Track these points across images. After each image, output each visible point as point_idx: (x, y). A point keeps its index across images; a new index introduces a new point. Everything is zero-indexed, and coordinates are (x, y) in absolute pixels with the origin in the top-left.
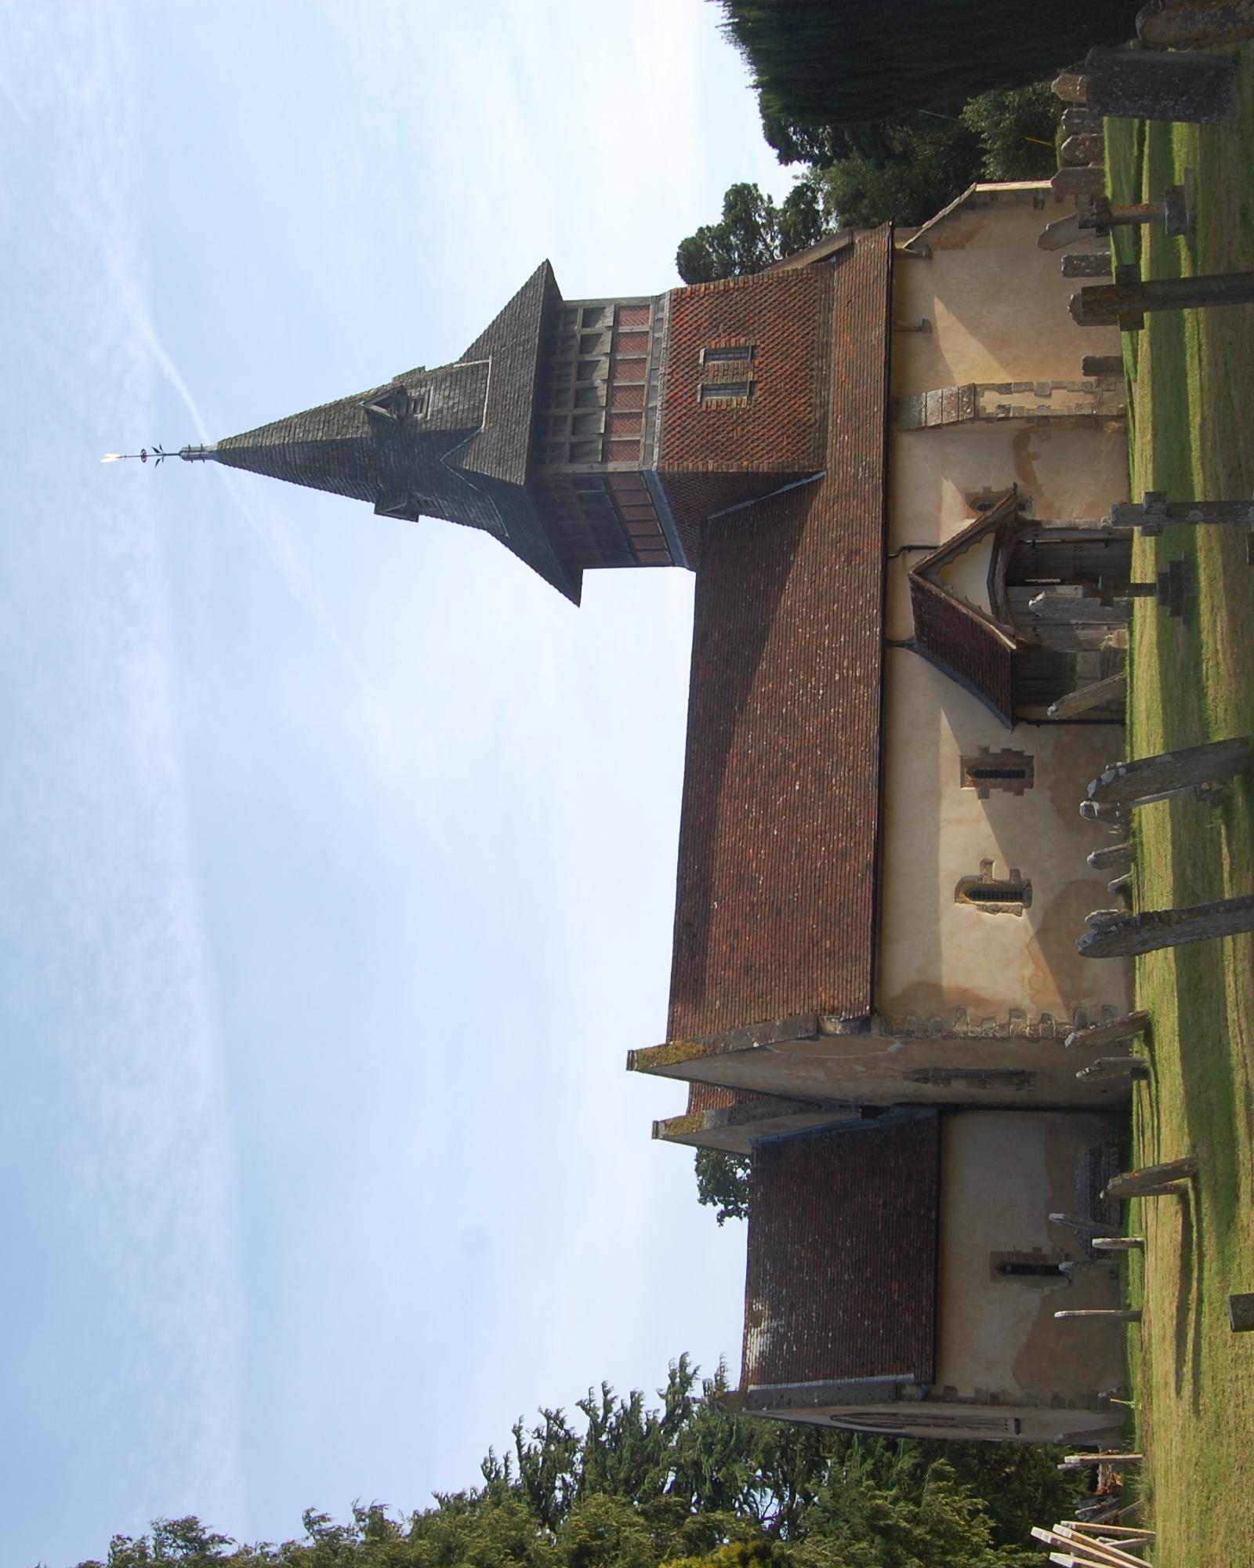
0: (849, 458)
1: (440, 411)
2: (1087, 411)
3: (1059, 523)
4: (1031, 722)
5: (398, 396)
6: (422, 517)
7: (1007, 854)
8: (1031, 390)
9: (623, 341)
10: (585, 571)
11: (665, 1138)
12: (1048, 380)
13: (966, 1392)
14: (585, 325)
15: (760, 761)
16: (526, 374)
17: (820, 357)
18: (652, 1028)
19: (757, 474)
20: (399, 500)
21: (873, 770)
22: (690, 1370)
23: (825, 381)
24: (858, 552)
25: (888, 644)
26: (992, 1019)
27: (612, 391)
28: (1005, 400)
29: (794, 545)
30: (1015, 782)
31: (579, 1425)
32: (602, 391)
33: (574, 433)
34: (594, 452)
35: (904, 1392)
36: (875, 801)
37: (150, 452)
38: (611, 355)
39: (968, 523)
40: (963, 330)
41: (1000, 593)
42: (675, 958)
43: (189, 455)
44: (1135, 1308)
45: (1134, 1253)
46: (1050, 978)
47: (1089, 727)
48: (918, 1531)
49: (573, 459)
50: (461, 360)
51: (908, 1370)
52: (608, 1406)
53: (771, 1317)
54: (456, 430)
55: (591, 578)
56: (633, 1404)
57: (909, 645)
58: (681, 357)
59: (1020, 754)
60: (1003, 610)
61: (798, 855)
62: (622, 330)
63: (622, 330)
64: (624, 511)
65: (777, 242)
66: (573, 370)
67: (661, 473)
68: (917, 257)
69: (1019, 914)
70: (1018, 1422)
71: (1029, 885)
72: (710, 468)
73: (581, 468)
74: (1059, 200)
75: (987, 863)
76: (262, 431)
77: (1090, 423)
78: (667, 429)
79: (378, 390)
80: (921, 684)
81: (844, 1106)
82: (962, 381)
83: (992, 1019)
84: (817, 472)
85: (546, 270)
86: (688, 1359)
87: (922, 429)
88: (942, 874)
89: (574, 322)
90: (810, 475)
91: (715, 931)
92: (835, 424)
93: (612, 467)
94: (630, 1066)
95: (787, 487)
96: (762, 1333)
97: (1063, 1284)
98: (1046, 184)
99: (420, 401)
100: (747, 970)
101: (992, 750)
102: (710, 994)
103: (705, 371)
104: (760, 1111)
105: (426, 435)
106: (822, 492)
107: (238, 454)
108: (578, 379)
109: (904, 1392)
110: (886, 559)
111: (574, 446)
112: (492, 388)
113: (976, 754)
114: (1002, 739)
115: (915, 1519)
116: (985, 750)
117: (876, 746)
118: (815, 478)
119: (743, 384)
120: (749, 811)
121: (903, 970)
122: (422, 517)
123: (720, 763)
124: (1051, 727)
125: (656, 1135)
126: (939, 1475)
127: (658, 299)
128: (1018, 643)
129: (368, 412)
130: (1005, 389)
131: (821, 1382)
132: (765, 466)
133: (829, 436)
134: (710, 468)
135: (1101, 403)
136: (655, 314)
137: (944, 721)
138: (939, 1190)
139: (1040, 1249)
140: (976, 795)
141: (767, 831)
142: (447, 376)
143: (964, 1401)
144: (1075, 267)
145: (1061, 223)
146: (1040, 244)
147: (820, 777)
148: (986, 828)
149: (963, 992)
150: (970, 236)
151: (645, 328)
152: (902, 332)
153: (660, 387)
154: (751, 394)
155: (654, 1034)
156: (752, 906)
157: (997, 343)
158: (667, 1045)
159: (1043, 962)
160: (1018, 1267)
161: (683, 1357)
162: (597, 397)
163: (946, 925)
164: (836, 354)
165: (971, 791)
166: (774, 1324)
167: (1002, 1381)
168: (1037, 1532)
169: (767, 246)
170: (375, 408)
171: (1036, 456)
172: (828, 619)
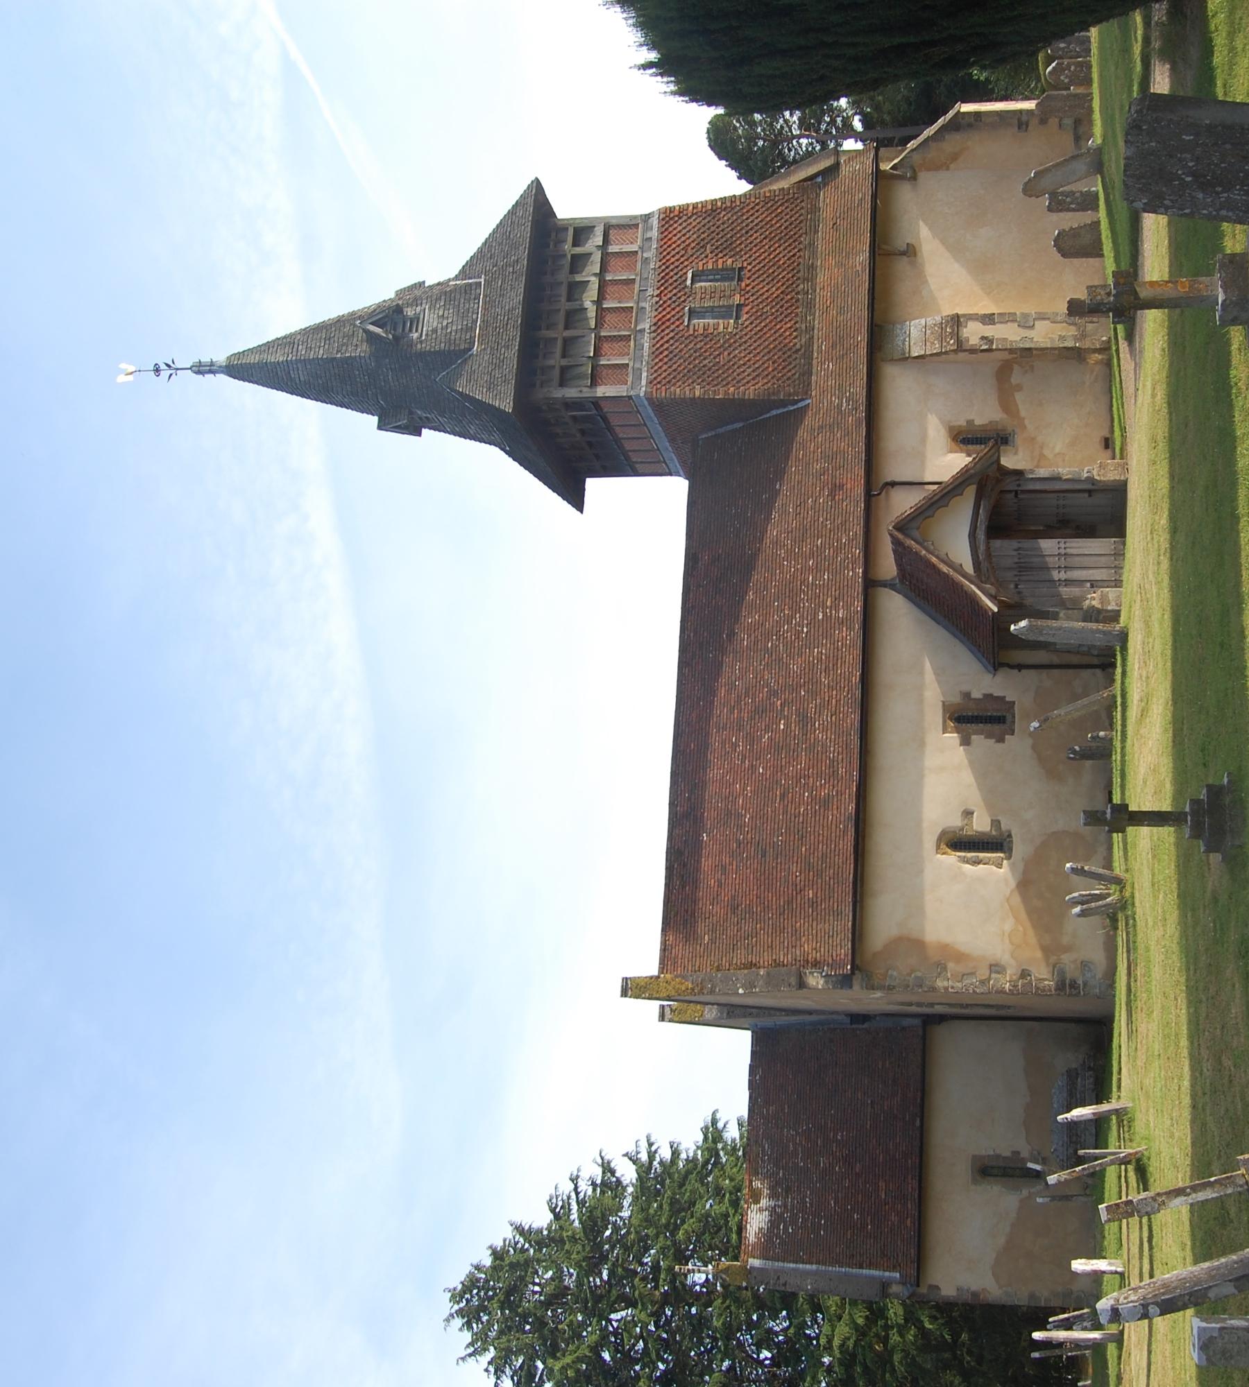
0: (833, 387)
1: (435, 331)
2: (1070, 344)
3: (1043, 472)
4: (1011, 667)
5: (392, 317)
6: (425, 431)
7: (989, 806)
8: (1014, 321)
9: (613, 262)
11: (671, 1021)
12: (1031, 308)
14: (575, 244)
15: (747, 695)
16: (515, 297)
17: (806, 280)
18: (646, 960)
19: (744, 400)
20: (402, 415)
21: (856, 717)
22: (720, 1125)
23: (810, 305)
24: (841, 487)
25: (871, 584)
26: (972, 974)
27: (601, 312)
28: (989, 331)
29: (780, 474)
30: (996, 728)
31: (627, 1173)
33: (564, 356)
34: (581, 376)
35: (891, 1291)
36: (857, 750)
37: (163, 367)
38: (601, 275)
40: (947, 254)
41: (982, 548)
42: (667, 885)
43: (201, 369)
46: (1031, 932)
47: (1070, 671)
49: (563, 383)
50: (456, 278)
51: (894, 1269)
52: (652, 1156)
54: (449, 351)
55: (594, 487)
56: (673, 1154)
57: (890, 585)
58: (669, 278)
60: (985, 565)
61: (783, 796)
62: (613, 248)
63: (613, 248)
64: (617, 429)
65: (795, 118)
66: (563, 291)
69: (1000, 866)
71: (1010, 836)
72: (697, 394)
73: (571, 393)
74: (1043, 121)
75: (968, 814)
76: (268, 346)
77: (1075, 355)
78: (656, 353)
79: (379, 305)
80: (900, 618)
82: (948, 311)
83: (972, 974)
84: (802, 400)
86: (718, 1116)
87: (905, 359)
88: (925, 825)
89: (565, 241)
90: (797, 402)
91: (706, 864)
92: (820, 352)
93: (601, 391)
94: (624, 993)
95: (774, 412)
96: (761, 1210)
98: (1030, 105)
99: (415, 320)
100: (734, 909)
101: (973, 696)
102: (701, 927)
103: (692, 293)
105: (422, 355)
108: (569, 300)
109: (891, 1291)
110: (869, 496)
111: (564, 370)
112: (485, 309)
113: (957, 699)
114: (983, 683)
116: (967, 695)
117: (858, 693)
118: (801, 405)
120: (736, 745)
121: (885, 923)
122: (425, 431)
123: (715, 670)
124: (1032, 672)
127: (647, 217)
128: (1000, 604)
129: (366, 331)
130: (988, 319)
131: (814, 1267)
132: (751, 392)
133: (815, 362)
134: (697, 394)
135: (1083, 336)
136: (644, 232)
137: (928, 665)
138: (923, 1099)
139: (1018, 1153)
140: (958, 741)
141: (753, 768)
142: (444, 294)
144: (1060, 203)
145: (1048, 170)
146: (1025, 191)
147: (804, 720)
148: (968, 777)
149: (944, 948)
150: (954, 157)
151: (634, 248)
152: (886, 254)
153: (648, 309)
154: (737, 318)
155: (648, 965)
157: (981, 267)
158: (658, 977)
159: (1023, 915)
160: (990, 1170)
161: (714, 1114)
162: (587, 319)
163: (929, 875)
164: (821, 278)
166: (772, 1203)
169: (786, 121)
170: (372, 328)
171: (1019, 388)
172: (812, 555)
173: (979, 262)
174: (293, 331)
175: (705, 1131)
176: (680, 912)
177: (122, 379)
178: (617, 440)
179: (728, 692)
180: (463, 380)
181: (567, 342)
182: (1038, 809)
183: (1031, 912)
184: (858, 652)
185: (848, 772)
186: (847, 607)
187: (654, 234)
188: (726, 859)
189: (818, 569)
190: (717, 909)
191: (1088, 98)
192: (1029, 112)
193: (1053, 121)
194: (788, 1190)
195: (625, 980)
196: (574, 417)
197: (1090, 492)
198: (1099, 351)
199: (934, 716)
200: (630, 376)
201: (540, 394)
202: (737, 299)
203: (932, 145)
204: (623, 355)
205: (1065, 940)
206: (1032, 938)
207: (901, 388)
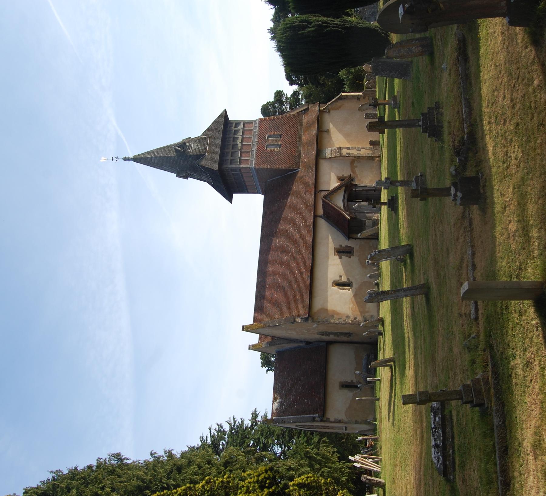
0: (306, 166)
1: (195, 149)
2: (370, 155)
4: (353, 239)
5: (183, 145)
7: (346, 274)
9: (246, 132)
10: (234, 195)
11: (252, 349)
12: (360, 146)
13: (332, 419)
14: (235, 127)
16: (219, 140)
18: (249, 320)
22: (257, 413)
23: (300, 145)
24: (308, 191)
25: (315, 216)
27: (242, 145)
28: (349, 151)
29: (290, 189)
31: (227, 428)
32: (239, 145)
37: (114, 158)
38: (242, 136)
39: (338, 184)
41: (346, 203)
43: (125, 159)
44: (378, 397)
45: (378, 382)
48: (318, 458)
49: (231, 164)
51: (317, 413)
52: (235, 422)
53: (280, 399)
55: (235, 196)
57: (321, 217)
58: (261, 137)
59: (350, 247)
60: (346, 208)
61: (290, 273)
62: (245, 129)
63: (245, 129)
66: (232, 139)
67: (255, 168)
68: (326, 112)
70: (346, 428)
73: (233, 166)
74: (364, 98)
75: (341, 276)
77: (371, 158)
78: (257, 156)
80: (323, 226)
81: (301, 341)
85: (225, 112)
87: (326, 158)
88: (329, 279)
90: (296, 170)
91: (267, 293)
93: (242, 166)
94: (243, 330)
97: (359, 390)
98: (361, 94)
99: (190, 146)
103: (267, 141)
104: (278, 342)
105: (191, 156)
106: (299, 175)
107: (137, 159)
110: (316, 193)
113: (338, 247)
114: (345, 243)
115: (317, 454)
116: (341, 246)
117: (312, 244)
119: (278, 145)
121: (318, 304)
123: (271, 242)
125: (249, 349)
126: (324, 442)
127: (255, 121)
128: (350, 217)
129: (175, 149)
130: (348, 148)
132: (283, 167)
135: (374, 153)
137: (330, 238)
141: (281, 266)
142: (197, 140)
143: (332, 422)
147: (296, 252)
148: (341, 267)
149: (334, 311)
150: (340, 107)
152: (321, 132)
156: (277, 286)
157: (347, 136)
163: (329, 293)
164: (303, 138)
165: (337, 257)
167: (342, 416)
168: (350, 457)
171: (356, 167)
173: (345, 135)
174: (171, 144)
175: (252, 414)
176: (259, 308)
177: (101, 161)
178: (244, 181)
179: (275, 247)
180: (203, 163)
181: (232, 153)
182: (359, 276)
183: (357, 302)
184: (312, 233)
185: (309, 265)
186: (309, 222)
187: (257, 125)
188: (273, 291)
189: (301, 213)
190: (270, 305)
191: (375, 91)
192: (361, 95)
193: (367, 98)
194: (286, 396)
195: (243, 326)
196: (233, 174)
197: (375, 190)
198: (377, 157)
199: (331, 251)
200: (249, 162)
201: (225, 166)
202: (280, 143)
203: (334, 103)
204: (248, 157)
205: (367, 310)
206: (357, 310)
207: (324, 166)
